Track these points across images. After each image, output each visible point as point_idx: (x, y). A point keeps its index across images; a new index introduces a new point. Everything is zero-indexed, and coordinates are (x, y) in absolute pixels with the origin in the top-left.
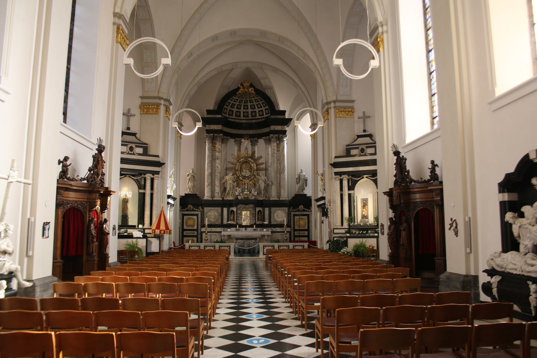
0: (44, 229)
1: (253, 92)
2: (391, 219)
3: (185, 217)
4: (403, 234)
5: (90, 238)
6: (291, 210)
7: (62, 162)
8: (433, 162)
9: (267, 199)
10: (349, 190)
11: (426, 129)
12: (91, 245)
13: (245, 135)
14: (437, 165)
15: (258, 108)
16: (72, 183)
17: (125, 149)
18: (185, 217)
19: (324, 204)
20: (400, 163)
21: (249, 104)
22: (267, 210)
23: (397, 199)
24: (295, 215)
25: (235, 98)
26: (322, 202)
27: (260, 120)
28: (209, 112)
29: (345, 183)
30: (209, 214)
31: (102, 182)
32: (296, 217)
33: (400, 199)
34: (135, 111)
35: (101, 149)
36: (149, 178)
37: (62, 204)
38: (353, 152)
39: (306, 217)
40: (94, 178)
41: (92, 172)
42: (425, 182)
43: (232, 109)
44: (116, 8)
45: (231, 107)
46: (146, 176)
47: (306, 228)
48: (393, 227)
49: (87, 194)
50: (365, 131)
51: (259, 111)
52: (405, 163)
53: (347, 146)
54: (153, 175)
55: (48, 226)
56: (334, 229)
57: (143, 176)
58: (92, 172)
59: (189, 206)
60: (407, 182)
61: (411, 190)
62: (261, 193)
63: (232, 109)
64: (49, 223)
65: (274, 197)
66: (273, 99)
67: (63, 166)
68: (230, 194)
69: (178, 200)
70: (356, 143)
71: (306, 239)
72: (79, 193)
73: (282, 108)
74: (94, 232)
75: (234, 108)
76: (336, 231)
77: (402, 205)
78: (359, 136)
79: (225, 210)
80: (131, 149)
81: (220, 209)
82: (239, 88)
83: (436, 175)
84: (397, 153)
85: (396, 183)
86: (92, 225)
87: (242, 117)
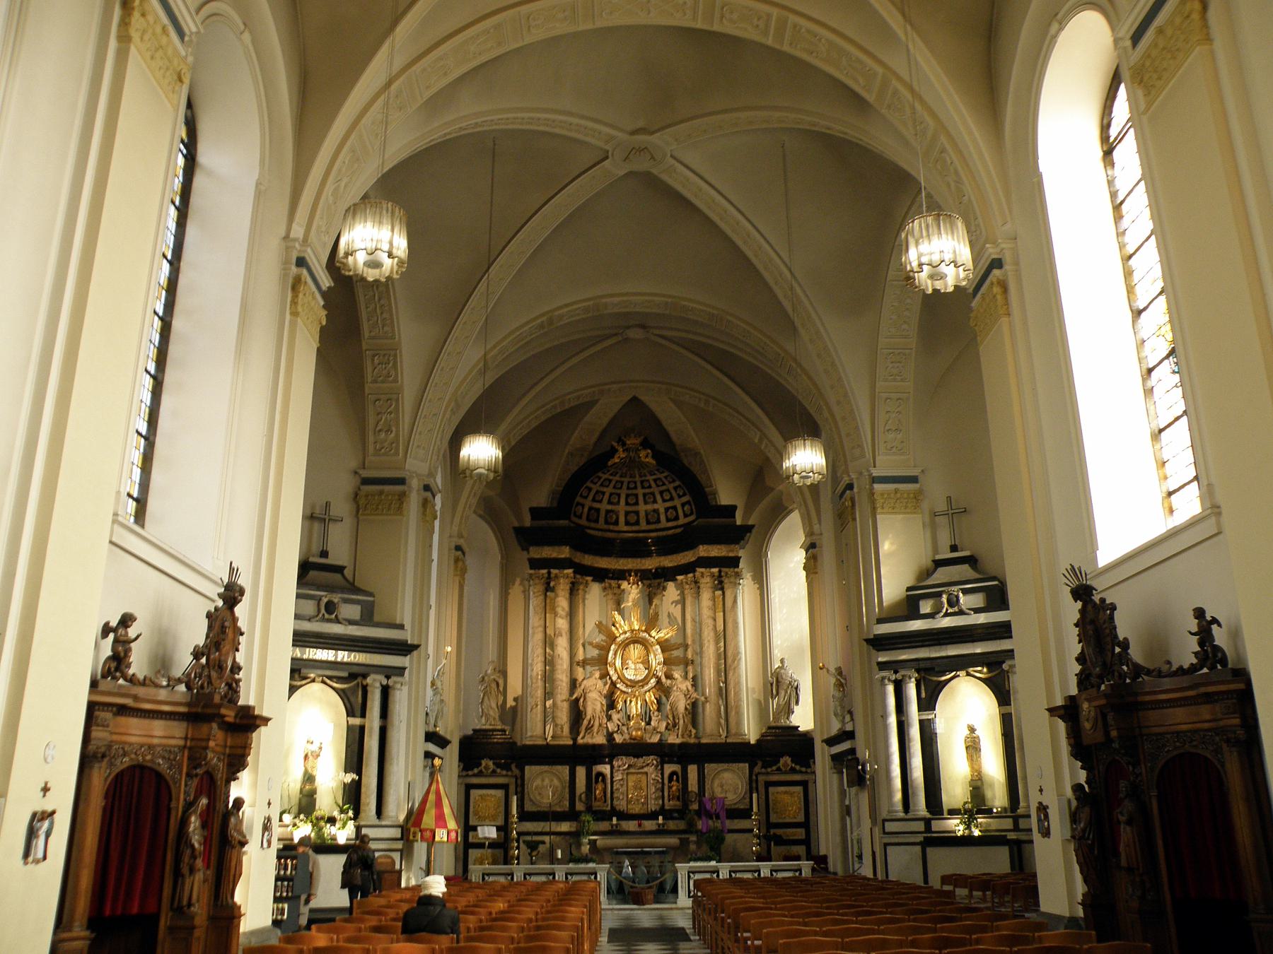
0: (31, 833)
1: (649, 460)
2: (1077, 788)
3: (475, 793)
4: (1126, 834)
5: (186, 859)
6: (757, 770)
7: (115, 630)
8: (1199, 613)
9: (692, 741)
10: (921, 708)
11: (1153, 526)
12: (188, 882)
13: (629, 571)
14: (1215, 621)
15: (664, 501)
16: (140, 691)
17: (309, 608)
18: (475, 793)
19: (852, 751)
20: (1096, 619)
21: (640, 492)
22: (693, 770)
23: (1095, 727)
24: (769, 784)
25: (605, 476)
26: (845, 746)
27: (671, 532)
28: (536, 513)
29: (911, 690)
30: (538, 782)
31: (233, 688)
32: (771, 789)
33: (1105, 725)
34: (341, 508)
35: (232, 595)
36: (378, 685)
37: (104, 756)
38: (926, 607)
39: (799, 789)
40: (209, 676)
41: (204, 660)
42: (1181, 671)
43: (596, 505)
44: (294, 226)
45: (594, 500)
46: (369, 680)
47: (801, 818)
48: (1085, 814)
49: (184, 724)
50: (954, 548)
51: (667, 510)
52: (1112, 618)
53: (909, 589)
54: (388, 677)
55: (46, 824)
56: (884, 821)
57: (359, 680)
58: (204, 660)
59: (484, 763)
60: (1122, 676)
61: (1140, 699)
62: (675, 725)
63: (596, 505)
64: (53, 813)
65: (711, 730)
66: (702, 478)
67: (116, 641)
68: (595, 729)
69: (454, 749)
70: (929, 582)
71: (801, 850)
72: (175, 723)
73: (725, 499)
74: (196, 840)
75: (600, 501)
76: (890, 827)
77: (1116, 745)
78: (939, 563)
79: (581, 772)
80: (330, 607)
81: (565, 770)
82: (613, 452)
83: (1217, 649)
84: (1082, 592)
85: (1084, 680)
86: (193, 819)
87: (622, 526)
